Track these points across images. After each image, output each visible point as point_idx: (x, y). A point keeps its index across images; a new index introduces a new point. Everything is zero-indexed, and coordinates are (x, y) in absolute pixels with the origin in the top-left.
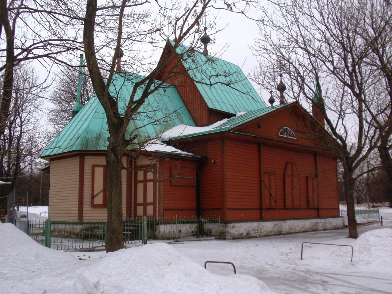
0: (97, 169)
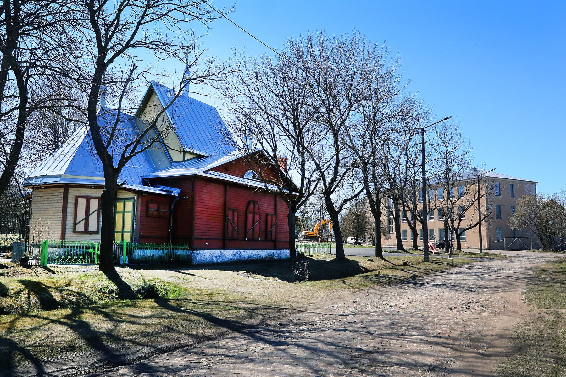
0: (80, 200)
